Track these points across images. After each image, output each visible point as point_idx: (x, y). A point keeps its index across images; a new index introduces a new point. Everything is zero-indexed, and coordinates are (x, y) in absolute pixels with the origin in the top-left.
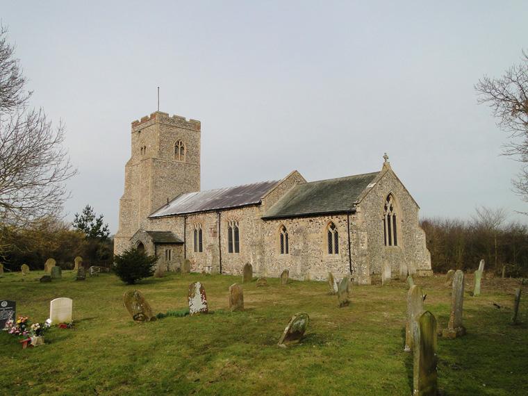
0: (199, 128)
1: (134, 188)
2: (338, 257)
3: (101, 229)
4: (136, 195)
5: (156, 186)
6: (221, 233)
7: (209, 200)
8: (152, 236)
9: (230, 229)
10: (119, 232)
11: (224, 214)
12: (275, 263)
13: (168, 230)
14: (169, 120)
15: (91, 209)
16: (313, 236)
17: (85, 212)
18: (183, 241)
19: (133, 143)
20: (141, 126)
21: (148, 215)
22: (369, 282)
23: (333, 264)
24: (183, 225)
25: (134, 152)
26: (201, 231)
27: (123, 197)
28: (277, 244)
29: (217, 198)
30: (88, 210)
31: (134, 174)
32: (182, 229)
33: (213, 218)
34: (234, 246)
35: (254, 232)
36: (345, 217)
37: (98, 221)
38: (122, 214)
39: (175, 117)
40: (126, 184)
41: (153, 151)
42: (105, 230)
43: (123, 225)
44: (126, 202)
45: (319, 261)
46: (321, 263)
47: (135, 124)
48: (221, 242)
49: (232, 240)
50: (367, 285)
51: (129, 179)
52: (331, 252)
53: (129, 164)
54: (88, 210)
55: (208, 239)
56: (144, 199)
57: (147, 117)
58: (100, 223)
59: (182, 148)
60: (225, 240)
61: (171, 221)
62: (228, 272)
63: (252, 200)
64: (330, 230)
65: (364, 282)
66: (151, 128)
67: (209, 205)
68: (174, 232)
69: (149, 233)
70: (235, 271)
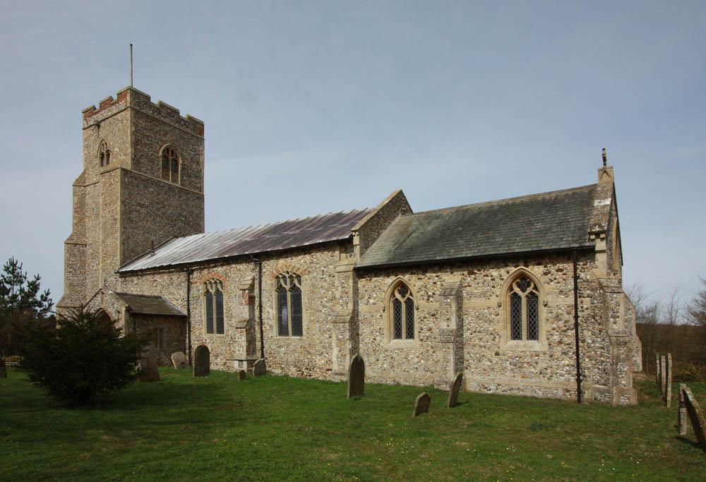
0: (201, 132)
1: (89, 223)
2: (535, 345)
3: (38, 297)
4: (94, 235)
5: (129, 219)
6: (263, 299)
7: (230, 242)
8: (127, 301)
9: (280, 290)
10: (64, 298)
11: (271, 267)
12: (400, 362)
13: (156, 294)
14: (152, 106)
15: (18, 265)
16: (473, 304)
17: (7, 269)
18: (185, 313)
19: (86, 147)
20: (99, 117)
21: (117, 268)
22: (634, 401)
23: (528, 359)
24: (185, 285)
25: (88, 161)
26: (219, 294)
27: (71, 238)
28: (385, 321)
29: (248, 239)
30: (12, 267)
31: (88, 200)
32: (183, 293)
33: (245, 273)
34: (293, 325)
35: (338, 295)
36: (569, 267)
37: (30, 284)
38: (69, 266)
39: (162, 105)
40: (74, 217)
41: (123, 156)
42: (44, 298)
43: (71, 286)
44: (76, 247)
45: (489, 354)
46: (495, 359)
47: (90, 112)
48: (264, 316)
49: (400, 319)
50: (631, 407)
51: (80, 209)
52: (516, 335)
53: (80, 184)
54: (12, 267)
55: (236, 310)
56: (109, 241)
57: (111, 99)
58: (34, 287)
59: (176, 162)
60: (270, 312)
61: (162, 279)
62: (278, 371)
63: (330, 236)
64: (398, 296)
65: (624, 401)
66: (118, 116)
67: (232, 249)
68: (166, 297)
69: (122, 296)
70: (293, 369)
